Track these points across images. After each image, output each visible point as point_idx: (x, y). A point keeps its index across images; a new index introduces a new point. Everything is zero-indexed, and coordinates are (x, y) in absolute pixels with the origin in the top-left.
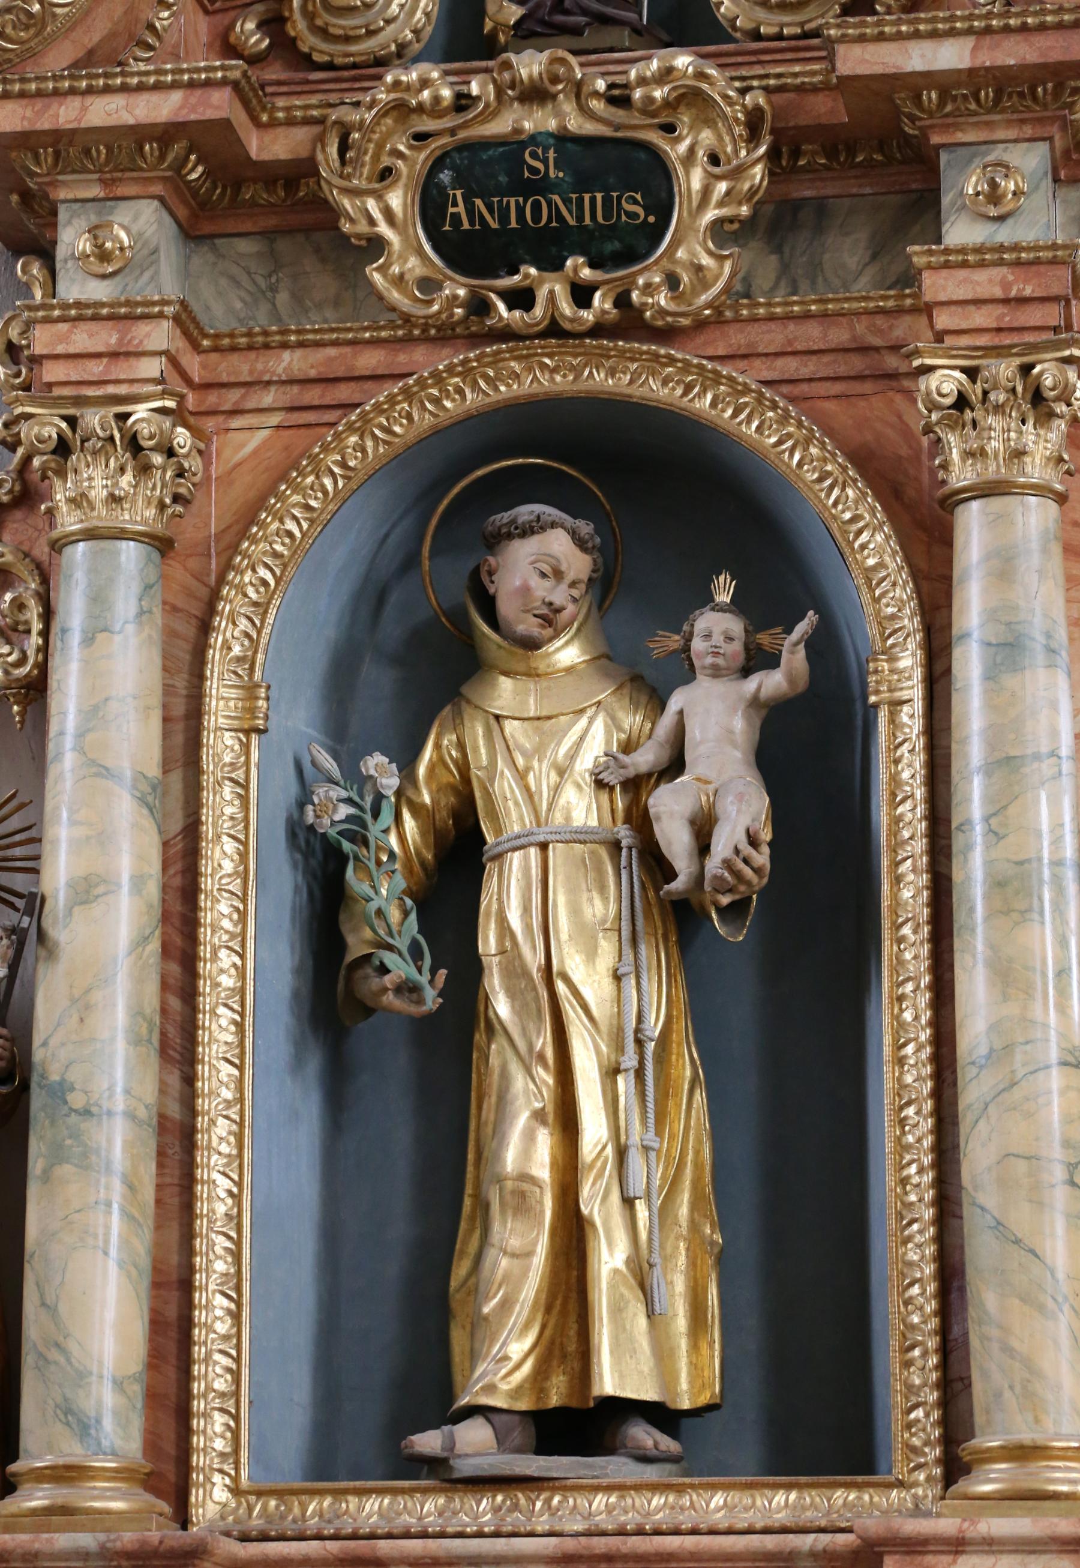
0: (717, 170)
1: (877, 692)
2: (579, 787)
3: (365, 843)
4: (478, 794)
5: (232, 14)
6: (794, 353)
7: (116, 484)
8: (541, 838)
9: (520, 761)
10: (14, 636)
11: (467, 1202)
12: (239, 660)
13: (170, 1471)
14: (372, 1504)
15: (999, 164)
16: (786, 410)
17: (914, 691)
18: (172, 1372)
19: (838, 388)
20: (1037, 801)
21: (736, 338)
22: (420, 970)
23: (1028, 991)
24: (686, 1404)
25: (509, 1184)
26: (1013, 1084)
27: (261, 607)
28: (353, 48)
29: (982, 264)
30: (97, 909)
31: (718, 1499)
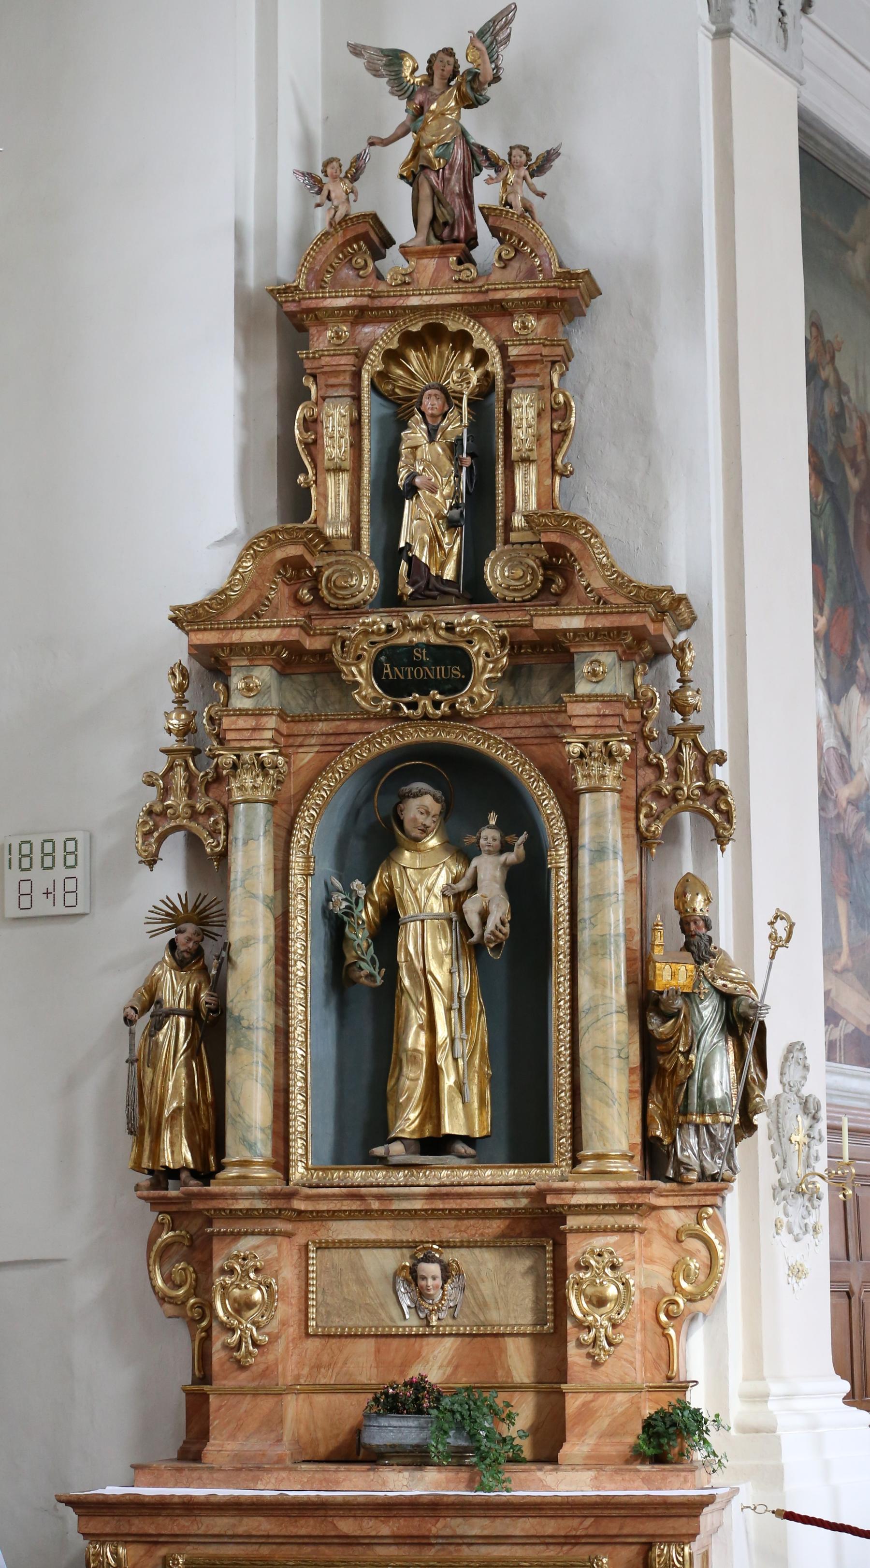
0: (489, 659)
1: (551, 863)
2: (436, 897)
3: (353, 916)
4: (397, 898)
5: (298, 585)
6: (520, 727)
7: (255, 781)
8: (422, 918)
9: (413, 885)
10: (214, 835)
11: (393, 1056)
12: (303, 846)
13: (282, 1161)
14: (358, 1174)
15: (596, 661)
16: (516, 752)
17: (564, 864)
18: (281, 1125)
19: (536, 741)
20: (609, 911)
21: (497, 721)
22: (374, 969)
23: (604, 985)
24: (477, 1136)
25: (410, 1053)
26: (598, 1020)
27: (312, 826)
28: (346, 602)
29: (589, 701)
30: (251, 949)
31: (489, 1172)
